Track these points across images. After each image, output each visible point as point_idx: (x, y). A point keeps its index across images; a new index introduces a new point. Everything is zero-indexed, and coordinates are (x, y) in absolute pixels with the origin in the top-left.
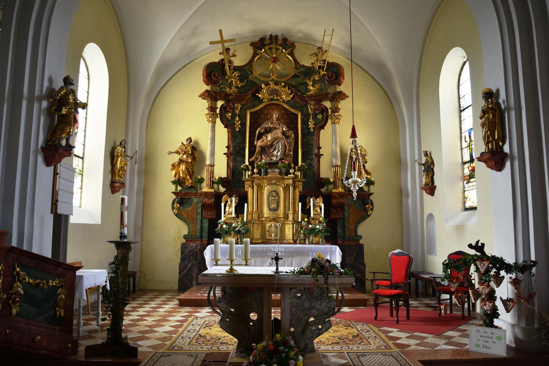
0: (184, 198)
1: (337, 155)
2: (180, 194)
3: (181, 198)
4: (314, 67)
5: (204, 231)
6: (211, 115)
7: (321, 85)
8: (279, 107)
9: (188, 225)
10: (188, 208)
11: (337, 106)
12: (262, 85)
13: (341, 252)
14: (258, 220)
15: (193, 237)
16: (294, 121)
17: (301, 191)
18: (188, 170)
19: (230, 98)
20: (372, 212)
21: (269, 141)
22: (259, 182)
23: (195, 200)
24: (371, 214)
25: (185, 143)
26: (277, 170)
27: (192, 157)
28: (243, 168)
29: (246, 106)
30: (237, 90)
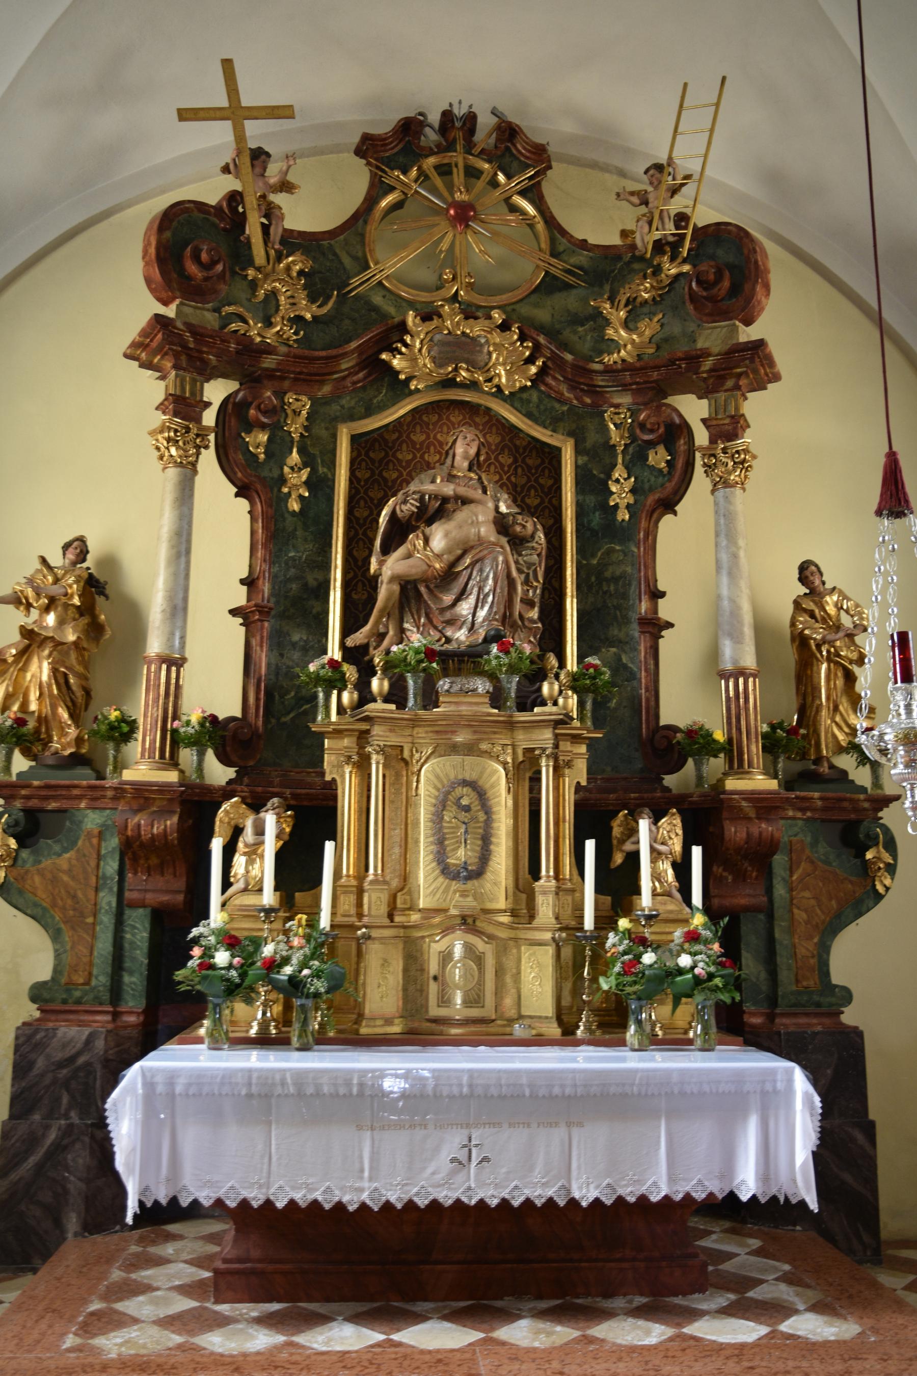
0: (43, 811)
1: (741, 623)
2: (23, 792)
3: (29, 813)
4: (633, 247)
5: (127, 964)
6: (176, 431)
7: (665, 321)
8: (477, 420)
9: (56, 936)
10: (60, 855)
11: (737, 408)
12: (405, 315)
13: (817, 1099)
14: (386, 921)
15: (77, 994)
16: (541, 481)
17: (584, 783)
18: (62, 681)
19: (265, 365)
20: (892, 879)
21: (438, 556)
22: (394, 740)
23: (92, 820)
24: (887, 889)
25: (56, 559)
26: (482, 685)
27: (85, 620)
28: (317, 674)
29: (335, 407)
30: (296, 333)
